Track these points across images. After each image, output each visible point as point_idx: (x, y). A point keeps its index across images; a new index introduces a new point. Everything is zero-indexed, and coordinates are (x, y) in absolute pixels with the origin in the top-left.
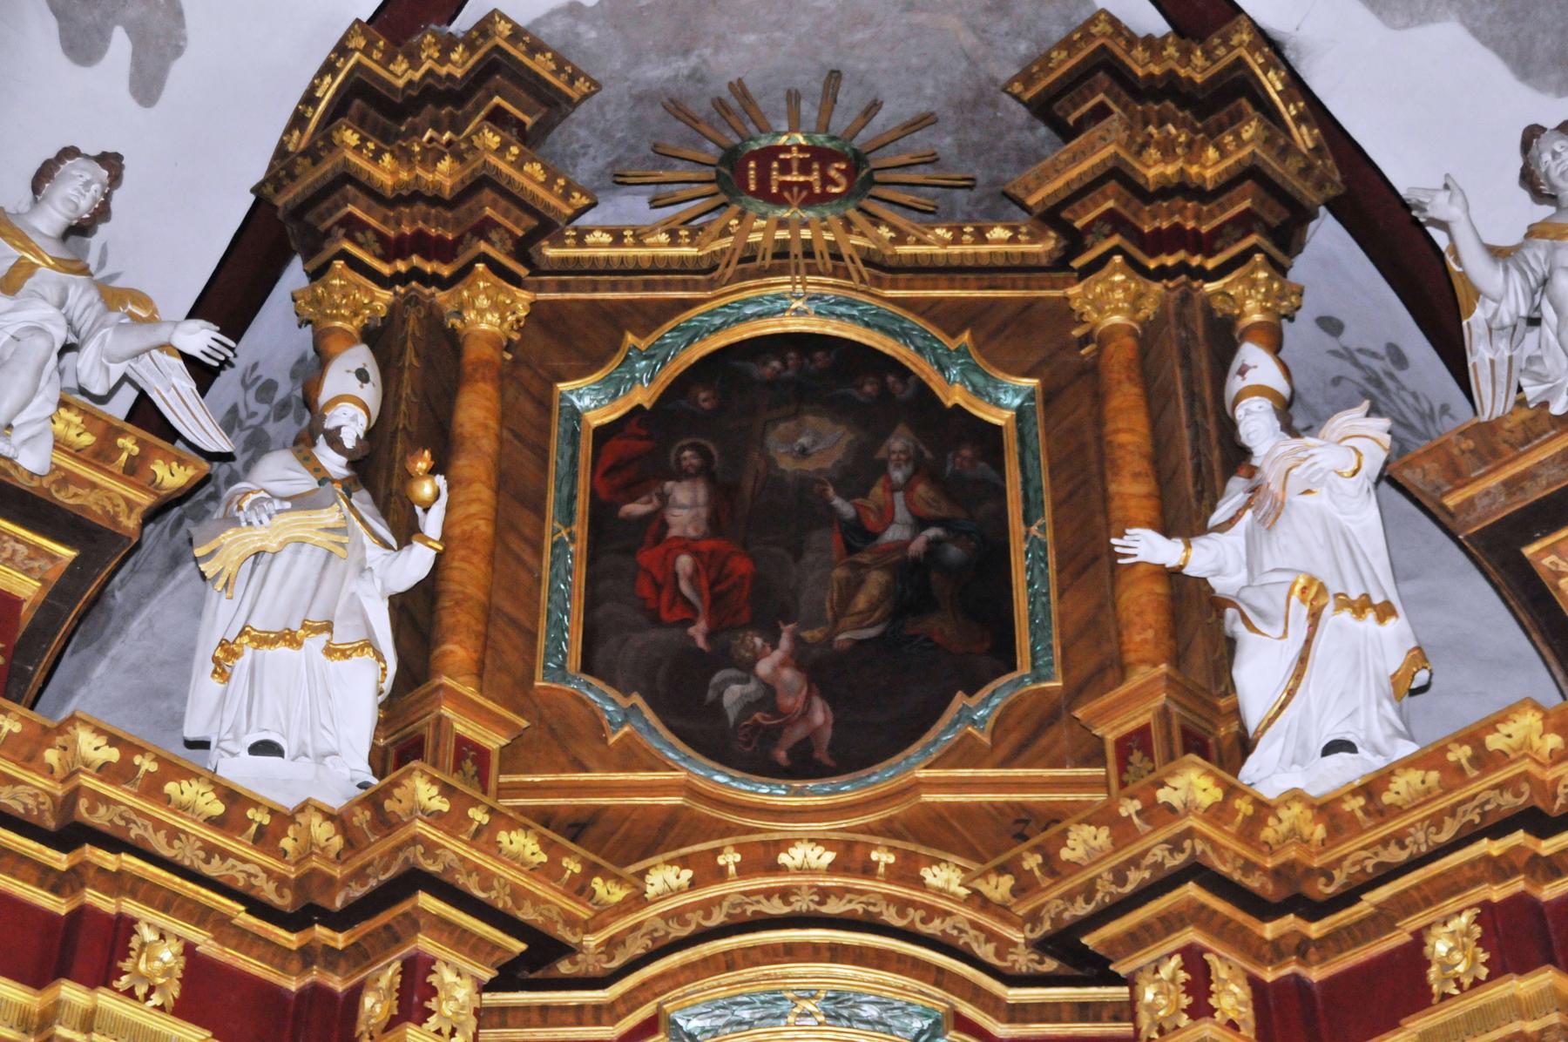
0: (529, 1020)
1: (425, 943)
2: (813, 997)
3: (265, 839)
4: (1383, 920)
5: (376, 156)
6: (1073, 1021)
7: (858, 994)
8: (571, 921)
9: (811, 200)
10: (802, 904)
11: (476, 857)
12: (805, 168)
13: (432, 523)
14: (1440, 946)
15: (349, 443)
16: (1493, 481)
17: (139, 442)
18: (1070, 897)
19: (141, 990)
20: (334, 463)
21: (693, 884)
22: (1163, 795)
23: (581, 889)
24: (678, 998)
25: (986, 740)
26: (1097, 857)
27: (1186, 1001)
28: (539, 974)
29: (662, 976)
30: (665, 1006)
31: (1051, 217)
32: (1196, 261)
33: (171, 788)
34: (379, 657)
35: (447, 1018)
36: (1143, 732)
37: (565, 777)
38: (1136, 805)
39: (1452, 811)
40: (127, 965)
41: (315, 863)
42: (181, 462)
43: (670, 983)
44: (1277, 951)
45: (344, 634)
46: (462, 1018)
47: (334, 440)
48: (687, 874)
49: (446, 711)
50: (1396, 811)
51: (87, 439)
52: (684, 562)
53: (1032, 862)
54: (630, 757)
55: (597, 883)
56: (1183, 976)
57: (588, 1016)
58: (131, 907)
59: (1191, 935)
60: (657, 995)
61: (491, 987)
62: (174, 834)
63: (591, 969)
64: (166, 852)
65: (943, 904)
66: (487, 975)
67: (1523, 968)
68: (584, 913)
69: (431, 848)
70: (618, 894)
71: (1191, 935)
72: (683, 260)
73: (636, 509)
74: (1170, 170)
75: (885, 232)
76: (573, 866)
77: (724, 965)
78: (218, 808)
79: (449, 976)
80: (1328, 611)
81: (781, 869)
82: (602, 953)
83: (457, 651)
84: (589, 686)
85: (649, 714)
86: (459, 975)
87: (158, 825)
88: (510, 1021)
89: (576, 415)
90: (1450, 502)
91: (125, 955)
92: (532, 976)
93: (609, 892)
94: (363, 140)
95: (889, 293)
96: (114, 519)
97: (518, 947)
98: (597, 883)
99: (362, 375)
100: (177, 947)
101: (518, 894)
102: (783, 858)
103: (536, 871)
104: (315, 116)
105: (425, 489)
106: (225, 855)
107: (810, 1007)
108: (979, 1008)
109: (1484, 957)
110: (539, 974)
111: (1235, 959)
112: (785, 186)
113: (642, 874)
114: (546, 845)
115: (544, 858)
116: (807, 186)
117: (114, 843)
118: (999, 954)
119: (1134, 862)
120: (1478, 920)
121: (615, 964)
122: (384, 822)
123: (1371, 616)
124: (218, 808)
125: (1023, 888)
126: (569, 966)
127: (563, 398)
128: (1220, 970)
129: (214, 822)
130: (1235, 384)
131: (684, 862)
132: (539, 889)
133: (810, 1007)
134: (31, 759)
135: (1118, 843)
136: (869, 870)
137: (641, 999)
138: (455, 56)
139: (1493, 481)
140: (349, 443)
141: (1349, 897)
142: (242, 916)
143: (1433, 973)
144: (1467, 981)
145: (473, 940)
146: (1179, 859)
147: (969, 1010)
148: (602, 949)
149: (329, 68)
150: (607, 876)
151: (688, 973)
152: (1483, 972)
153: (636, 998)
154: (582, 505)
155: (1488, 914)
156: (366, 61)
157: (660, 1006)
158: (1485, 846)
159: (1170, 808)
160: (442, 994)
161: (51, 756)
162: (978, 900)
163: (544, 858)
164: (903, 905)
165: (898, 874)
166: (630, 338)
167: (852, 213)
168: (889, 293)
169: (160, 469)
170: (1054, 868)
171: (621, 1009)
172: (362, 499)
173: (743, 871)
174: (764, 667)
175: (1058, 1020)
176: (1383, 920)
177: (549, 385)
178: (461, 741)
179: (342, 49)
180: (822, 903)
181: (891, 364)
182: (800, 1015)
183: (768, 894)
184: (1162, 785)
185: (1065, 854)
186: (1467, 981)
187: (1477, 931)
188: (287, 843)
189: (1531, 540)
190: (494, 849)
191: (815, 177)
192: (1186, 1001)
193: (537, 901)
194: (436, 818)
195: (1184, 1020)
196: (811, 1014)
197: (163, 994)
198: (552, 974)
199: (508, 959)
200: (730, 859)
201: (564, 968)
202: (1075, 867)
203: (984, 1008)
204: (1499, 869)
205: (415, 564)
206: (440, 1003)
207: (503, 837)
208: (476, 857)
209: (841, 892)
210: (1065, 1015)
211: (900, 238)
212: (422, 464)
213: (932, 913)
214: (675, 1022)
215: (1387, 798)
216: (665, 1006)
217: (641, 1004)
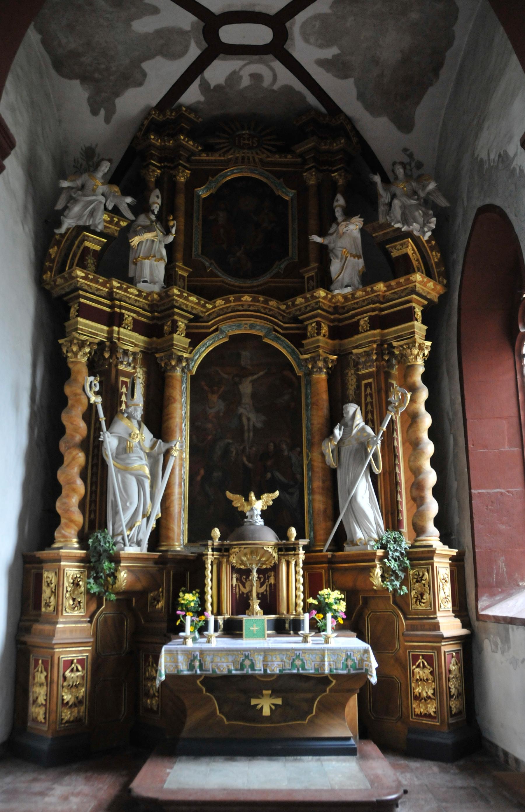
1: (176, 317)
3: (145, 298)
4: (353, 316)
5: (157, 141)
8: (202, 312)
9: (250, 148)
10: (245, 307)
11: (185, 302)
12: (248, 140)
13: (174, 230)
14: (362, 322)
15: (156, 213)
16: (381, 233)
17: (118, 219)
18: (296, 310)
19: (126, 327)
20: (153, 217)
21: (225, 304)
22: (315, 294)
23: (204, 306)
25: (282, 272)
26: (301, 303)
27: (316, 331)
31: (301, 155)
32: (330, 168)
33: (129, 290)
34: (165, 261)
36: (312, 276)
37: (199, 279)
38: (310, 295)
39: (367, 299)
40: (124, 322)
41: (155, 302)
42: (125, 222)
44: (333, 321)
45: (158, 256)
47: (153, 212)
48: (224, 302)
49: (177, 269)
50: (357, 298)
51: (109, 219)
52: (222, 231)
53: (290, 303)
54: (213, 274)
55: (207, 305)
56: (316, 327)
58: (123, 311)
59: (318, 319)
62: (130, 298)
64: (129, 302)
65: (272, 308)
67: (375, 329)
68: (204, 310)
69: (177, 301)
70: (211, 307)
71: (318, 319)
72: (221, 160)
73: (212, 217)
74: (327, 147)
75: (265, 155)
76: (202, 302)
78: (137, 293)
79: (180, 323)
80: (349, 258)
81: (242, 301)
83: (179, 255)
84: (203, 258)
85: (215, 264)
87: (127, 297)
89: (199, 196)
90: (374, 235)
91: (123, 321)
93: (209, 306)
94: (154, 137)
95: (266, 168)
96: (114, 234)
97: (192, 317)
98: (207, 305)
99: (158, 197)
100: (131, 318)
101: (192, 308)
102: (242, 299)
103: (197, 304)
104: (144, 129)
105: (171, 223)
106: (139, 301)
109: (369, 326)
111: (326, 322)
112: (244, 144)
113: (215, 302)
114: (197, 299)
115: (197, 301)
116: (248, 144)
117: (120, 300)
118: (283, 318)
119: (309, 305)
120: (369, 319)
122: (168, 296)
123: (356, 258)
124: (137, 293)
125: (288, 307)
127: (196, 192)
128: (323, 325)
129: (136, 296)
130: (335, 204)
131: (223, 300)
132: (196, 306)
133: (246, 326)
134: (105, 286)
135: (306, 302)
136: (258, 301)
138: (173, 114)
139: (381, 233)
140: (156, 213)
141: (348, 312)
142: (141, 311)
143: (360, 328)
144: (365, 330)
146: (317, 306)
147: (276, 328)
149: (146, 118)
150: (209, 303)
152: (368, 328)
154: (200, 218)
155: (371, 318)
156: (154, 116)
158: (372, 306)
159: (315, 296)
161: (108, 285)
162: (279, 309)
163: (197, 301)
164: (265, 308)
165: (263, 302)
166: (210, 178)
167: (258, 151)
168: (266, 168)
169: (121, 223)
170: (294, 305)
172: (159, 223)
173: (235, 301)
174: (238, 254)
176: (353, 316)
177: (194, 189)
178: (180, 275)
179: (149, 114)
180: (250, 307)
181: (265, 184)
183: (239, 305)
184: (315, 292)
185: (296, 303)
186: (365, 330)
187: (368, 321)
188: (149, 298)
189: (387, 245)
190: (188, 300)
191: (250, 142)
192: (316, 331)
193: (196, 309)
194: (177, 296)
195: (315, 335)
200: (232, 298)
201: (201, 320)
202: (298, 305)
204: (373, 310)
205: (170, 239)
207: (190, 298)
208: (185, 302)
209: (253, 305)
211: (268, 157)
212: (171, 218)
213: (270, 310)
215: (356, 296)
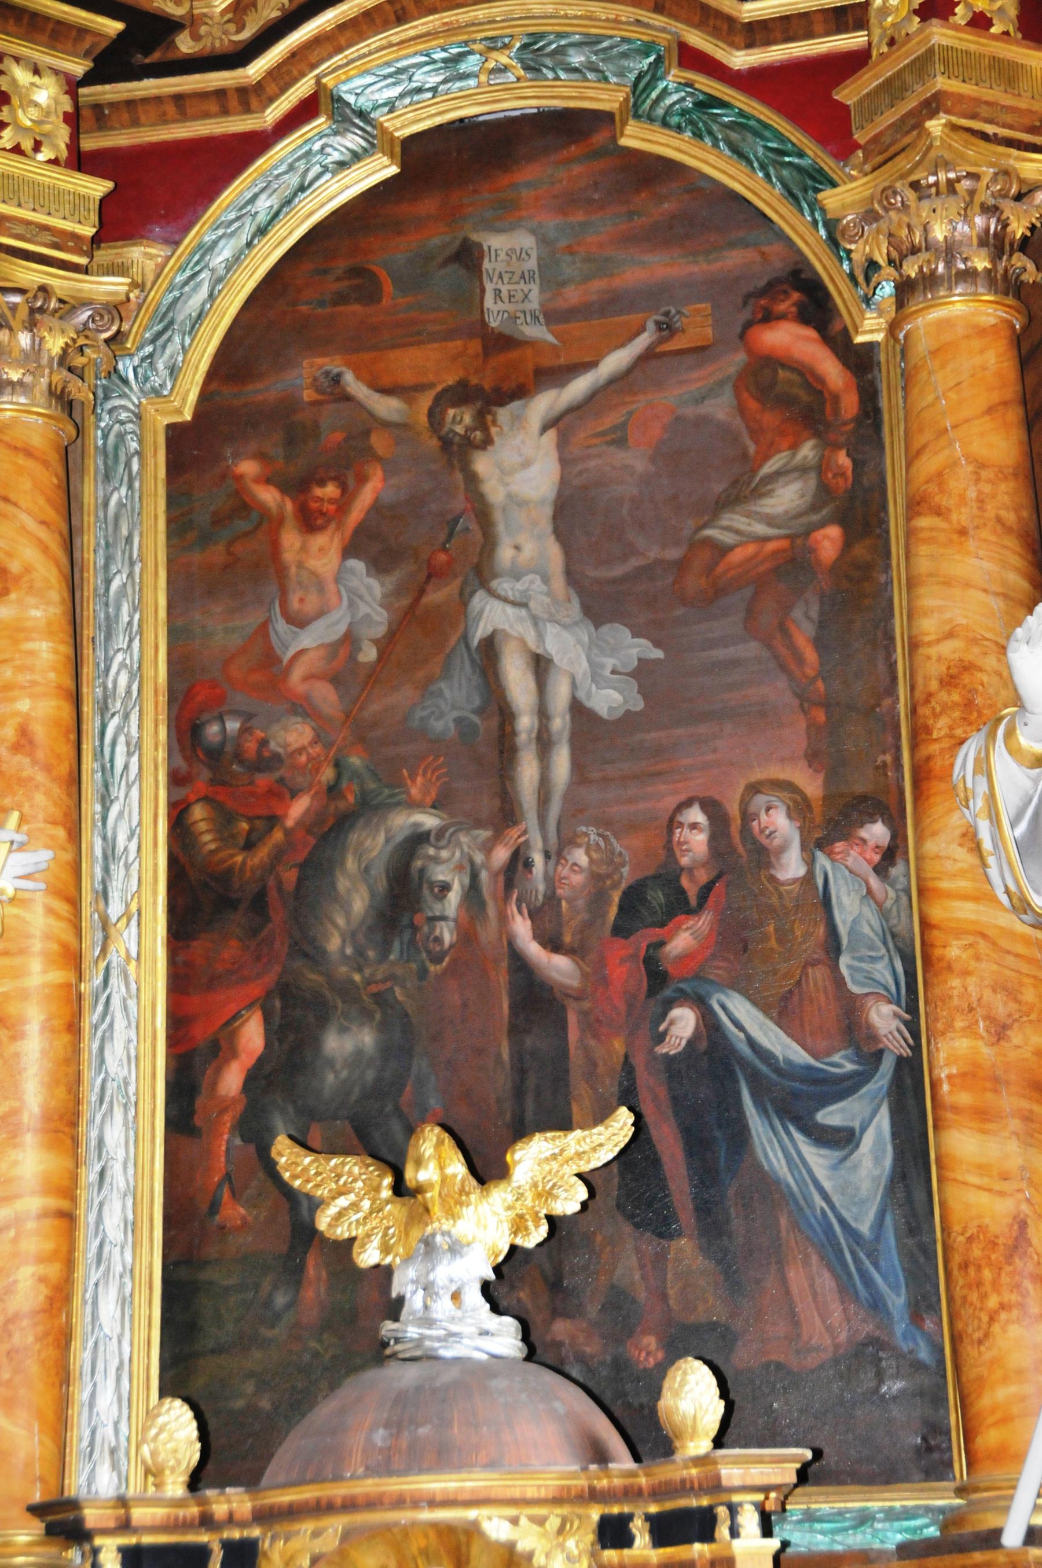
0: (164, 114)
2: (506, 46)
6: (828, 34)
7: (560, 35)
24: (340, 67)
28: (156, 56)
29: (315, 40)
30: (324, 81)
35: (27, 129)
43: (329, 48)
46: (47, 127)
57: (233, 102)
60: (314, 66)
61: (89, 79)
63: (217, 44)
66: (78, 68)
77: (393, 17)
79: (22, 75)
82: (229, 21)
86: (36, 72)
88: (143, 118)
92: (148, 61)
107: (504, 59)
108: (708, 34)
110: (156, 56)
121: (246, 35)
126: (191, 43)
137: (295, 73)
145: (50, 26)
147: (697, 39)
148: (230, 16)
151: (348, 34)
153: (289, 72)
157: (318, 80)
160: (15, 101)
171: (271, 88)
175: (809, 35)
182: (492, 71)
196: (504, 69)
197: (55, 147)
198: (170, 56)
199: (104, 45)
203: (716, 33)
206: (13, 113)
210: (818, 27)
214: (340, 99)
216: (324, 81)
217: (296, 80)
